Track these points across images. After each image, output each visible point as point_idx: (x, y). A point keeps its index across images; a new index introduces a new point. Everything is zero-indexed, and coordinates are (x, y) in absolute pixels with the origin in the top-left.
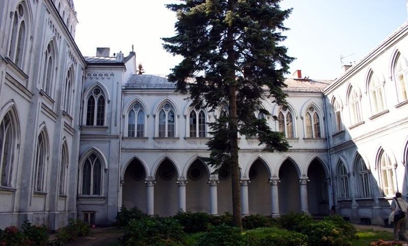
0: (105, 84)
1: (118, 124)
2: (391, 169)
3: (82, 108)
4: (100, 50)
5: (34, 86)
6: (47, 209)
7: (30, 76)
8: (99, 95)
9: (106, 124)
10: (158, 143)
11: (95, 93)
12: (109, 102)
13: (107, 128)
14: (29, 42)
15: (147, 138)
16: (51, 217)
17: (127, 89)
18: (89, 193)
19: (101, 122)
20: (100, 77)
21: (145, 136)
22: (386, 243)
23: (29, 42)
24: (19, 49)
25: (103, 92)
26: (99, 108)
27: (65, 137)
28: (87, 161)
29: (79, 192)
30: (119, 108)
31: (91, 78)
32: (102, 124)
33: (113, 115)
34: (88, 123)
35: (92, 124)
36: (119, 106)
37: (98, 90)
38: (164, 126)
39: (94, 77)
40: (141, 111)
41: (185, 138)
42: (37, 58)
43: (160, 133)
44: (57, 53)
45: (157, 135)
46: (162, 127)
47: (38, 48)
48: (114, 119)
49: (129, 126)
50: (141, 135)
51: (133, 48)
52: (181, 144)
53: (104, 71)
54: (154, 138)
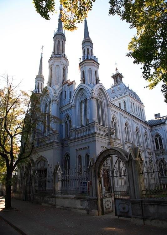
0: (160, 132)
2: (108, 170)
3: (153, 143)
4: (157, 116)
6: (148, 183)
8: (159, 137)
12: (163, 139)
14: (130, 133)
16: (149, 186)
18: (163, 176)
20: (157, 130)
22: (10, 163)
23: (130, 133)
24: (128, 136)
26: (160, 142)
28: (160, 163)
29: (159, 176)
31: (154, 131)
34: (157, 149)
37: (158, 135)
42: (133, 136)
48: (95, 189)
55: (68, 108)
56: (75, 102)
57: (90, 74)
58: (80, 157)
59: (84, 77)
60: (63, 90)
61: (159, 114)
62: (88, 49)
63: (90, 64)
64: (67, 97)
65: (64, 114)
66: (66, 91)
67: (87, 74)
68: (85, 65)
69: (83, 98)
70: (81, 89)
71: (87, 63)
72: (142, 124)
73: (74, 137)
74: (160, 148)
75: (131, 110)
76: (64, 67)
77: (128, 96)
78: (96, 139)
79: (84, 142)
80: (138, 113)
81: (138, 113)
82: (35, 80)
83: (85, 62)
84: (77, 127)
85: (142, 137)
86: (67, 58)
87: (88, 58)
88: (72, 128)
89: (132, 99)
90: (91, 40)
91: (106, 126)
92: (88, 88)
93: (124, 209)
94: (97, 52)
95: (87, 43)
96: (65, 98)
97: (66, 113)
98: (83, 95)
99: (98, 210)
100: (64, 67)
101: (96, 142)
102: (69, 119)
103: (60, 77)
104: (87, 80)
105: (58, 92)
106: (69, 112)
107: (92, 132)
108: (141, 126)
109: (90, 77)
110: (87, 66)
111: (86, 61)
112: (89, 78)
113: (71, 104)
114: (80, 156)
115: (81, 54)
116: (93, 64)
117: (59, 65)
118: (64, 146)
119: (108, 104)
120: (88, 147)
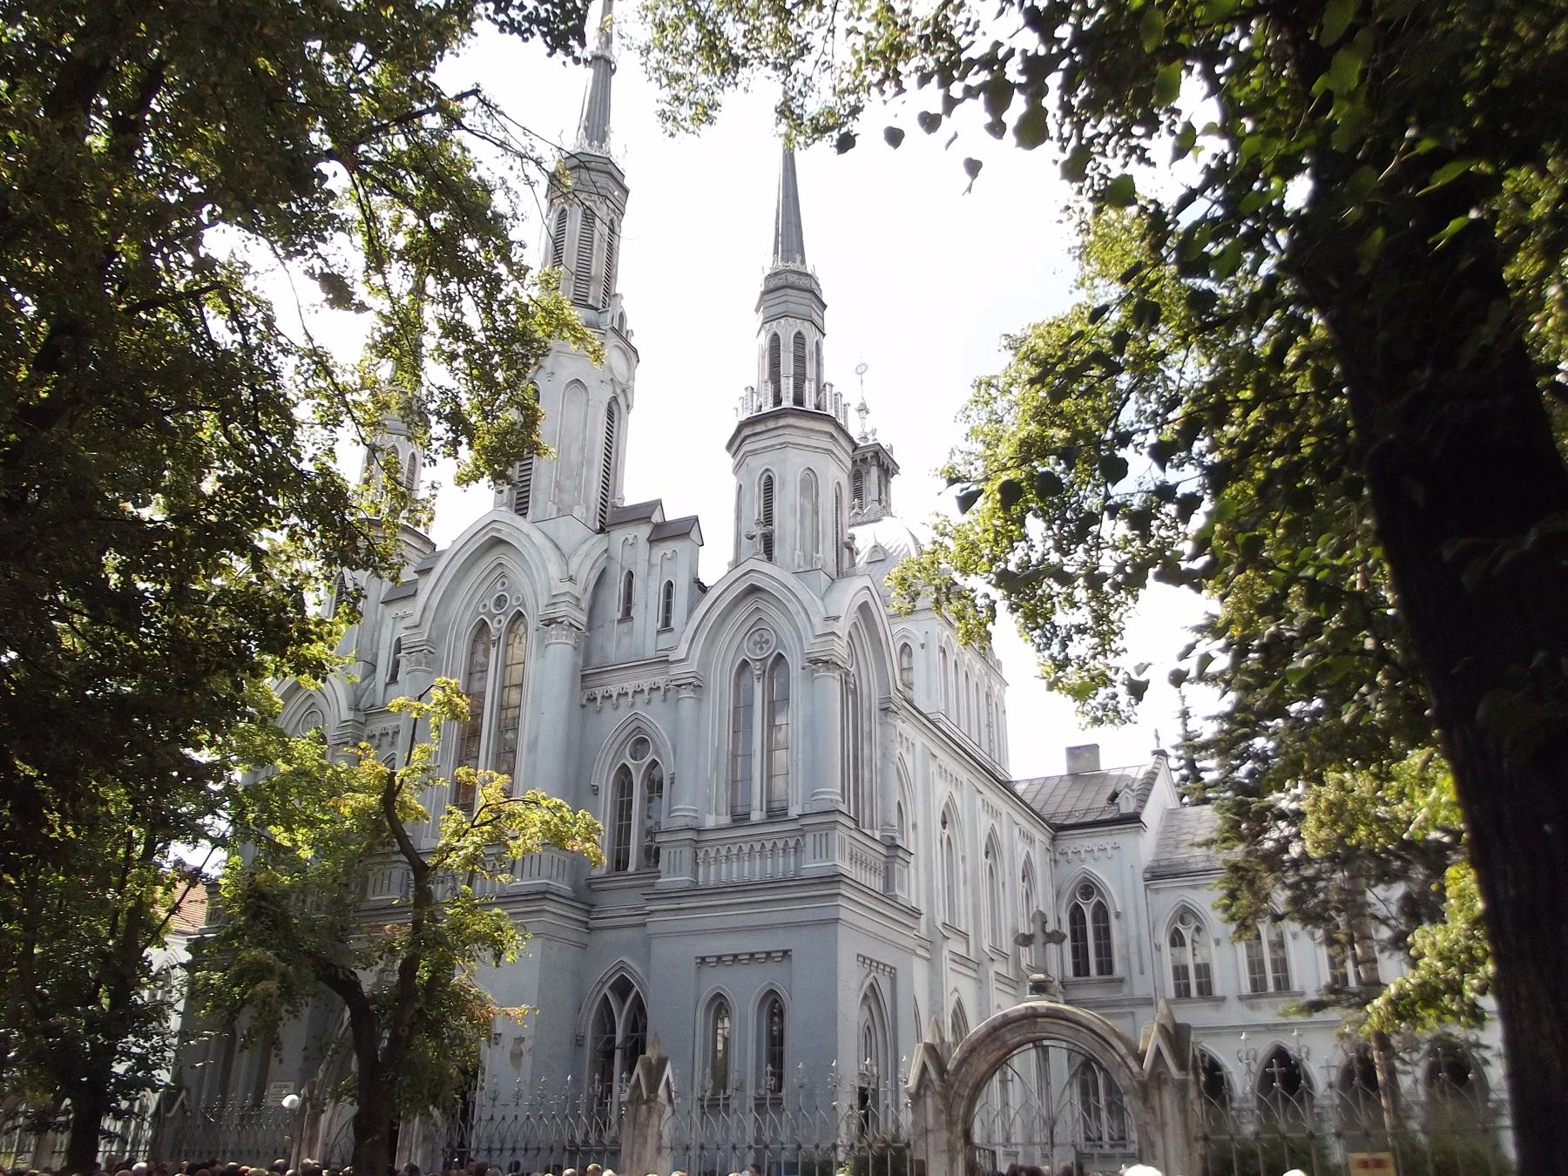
0: (1101, 872)
1: (1148, 970)
5: (979, 949)
7: (971, 933)
9: (1118, 969)
10: (1252, 1007)
11: (1082, 895)
12: (1118, 915)
13: (1121, 980)
15: (1223, 999)
17: (1157, 874)
19: (1106, 967)
21: (1218, 990)
25: (1100, 893)
27: (521, 508)
30: (1145, 932)
32: (1110, 971)
33: (1133, 948)
34: (1077, 973)
35: (1087, 973)
36: (1144, 922)
37: (1088, 888)
38: (1261, 963)
39: (1075, 858)
40: (1198, 930)
41: (1241, 998)
43: (1254, 983)
44: (1001, 853)
45: (1246, 988)
46: (1256, 966)
47: (975, 873)
49: (1176, 969)
50: (1206, 989)
51: (1158, 738)
52: (1235, 1014)
53: (1095, 840)
54: (1241, 998)
55: (630, 687)
56: (705, 664)
57: (809, 506)
60: (609, 558)
62: (799, 338)
63: (814, 441)
65: (612, 722)
66: (630, 574)
67: (787, 500)
68: (785, 445)
70: (754, 590)
73: (683, 879)
75: (942, 707)
76: (615, 399)
78: (843, 914)
80: (963, 712)
81: (963, 712)
83: (782, 422)
84: (710, 821)
85: (1014, 900)
86: (634, 341)
87: (799, 400)
88: (680, 823)
91: (872, 828)
92: (803, 596)
96: (627, 615)
97: (624, 714)
98: (757, 628)
100: (615, 399)
101: (841, 930)
102: (648, 759)
103: (590, 463)
104: (789, 541)
105: (586, 575)
106: (656, 718)
107: (812, 865)
108: (982, 815)
109: (808, 522)
111: (791, 421)
112: (802, 523)
113: (675, 670)
115: (748, 368)
116: (826, 443)
118: (593, 923)
119: (889, 700)
120: (785, 953)
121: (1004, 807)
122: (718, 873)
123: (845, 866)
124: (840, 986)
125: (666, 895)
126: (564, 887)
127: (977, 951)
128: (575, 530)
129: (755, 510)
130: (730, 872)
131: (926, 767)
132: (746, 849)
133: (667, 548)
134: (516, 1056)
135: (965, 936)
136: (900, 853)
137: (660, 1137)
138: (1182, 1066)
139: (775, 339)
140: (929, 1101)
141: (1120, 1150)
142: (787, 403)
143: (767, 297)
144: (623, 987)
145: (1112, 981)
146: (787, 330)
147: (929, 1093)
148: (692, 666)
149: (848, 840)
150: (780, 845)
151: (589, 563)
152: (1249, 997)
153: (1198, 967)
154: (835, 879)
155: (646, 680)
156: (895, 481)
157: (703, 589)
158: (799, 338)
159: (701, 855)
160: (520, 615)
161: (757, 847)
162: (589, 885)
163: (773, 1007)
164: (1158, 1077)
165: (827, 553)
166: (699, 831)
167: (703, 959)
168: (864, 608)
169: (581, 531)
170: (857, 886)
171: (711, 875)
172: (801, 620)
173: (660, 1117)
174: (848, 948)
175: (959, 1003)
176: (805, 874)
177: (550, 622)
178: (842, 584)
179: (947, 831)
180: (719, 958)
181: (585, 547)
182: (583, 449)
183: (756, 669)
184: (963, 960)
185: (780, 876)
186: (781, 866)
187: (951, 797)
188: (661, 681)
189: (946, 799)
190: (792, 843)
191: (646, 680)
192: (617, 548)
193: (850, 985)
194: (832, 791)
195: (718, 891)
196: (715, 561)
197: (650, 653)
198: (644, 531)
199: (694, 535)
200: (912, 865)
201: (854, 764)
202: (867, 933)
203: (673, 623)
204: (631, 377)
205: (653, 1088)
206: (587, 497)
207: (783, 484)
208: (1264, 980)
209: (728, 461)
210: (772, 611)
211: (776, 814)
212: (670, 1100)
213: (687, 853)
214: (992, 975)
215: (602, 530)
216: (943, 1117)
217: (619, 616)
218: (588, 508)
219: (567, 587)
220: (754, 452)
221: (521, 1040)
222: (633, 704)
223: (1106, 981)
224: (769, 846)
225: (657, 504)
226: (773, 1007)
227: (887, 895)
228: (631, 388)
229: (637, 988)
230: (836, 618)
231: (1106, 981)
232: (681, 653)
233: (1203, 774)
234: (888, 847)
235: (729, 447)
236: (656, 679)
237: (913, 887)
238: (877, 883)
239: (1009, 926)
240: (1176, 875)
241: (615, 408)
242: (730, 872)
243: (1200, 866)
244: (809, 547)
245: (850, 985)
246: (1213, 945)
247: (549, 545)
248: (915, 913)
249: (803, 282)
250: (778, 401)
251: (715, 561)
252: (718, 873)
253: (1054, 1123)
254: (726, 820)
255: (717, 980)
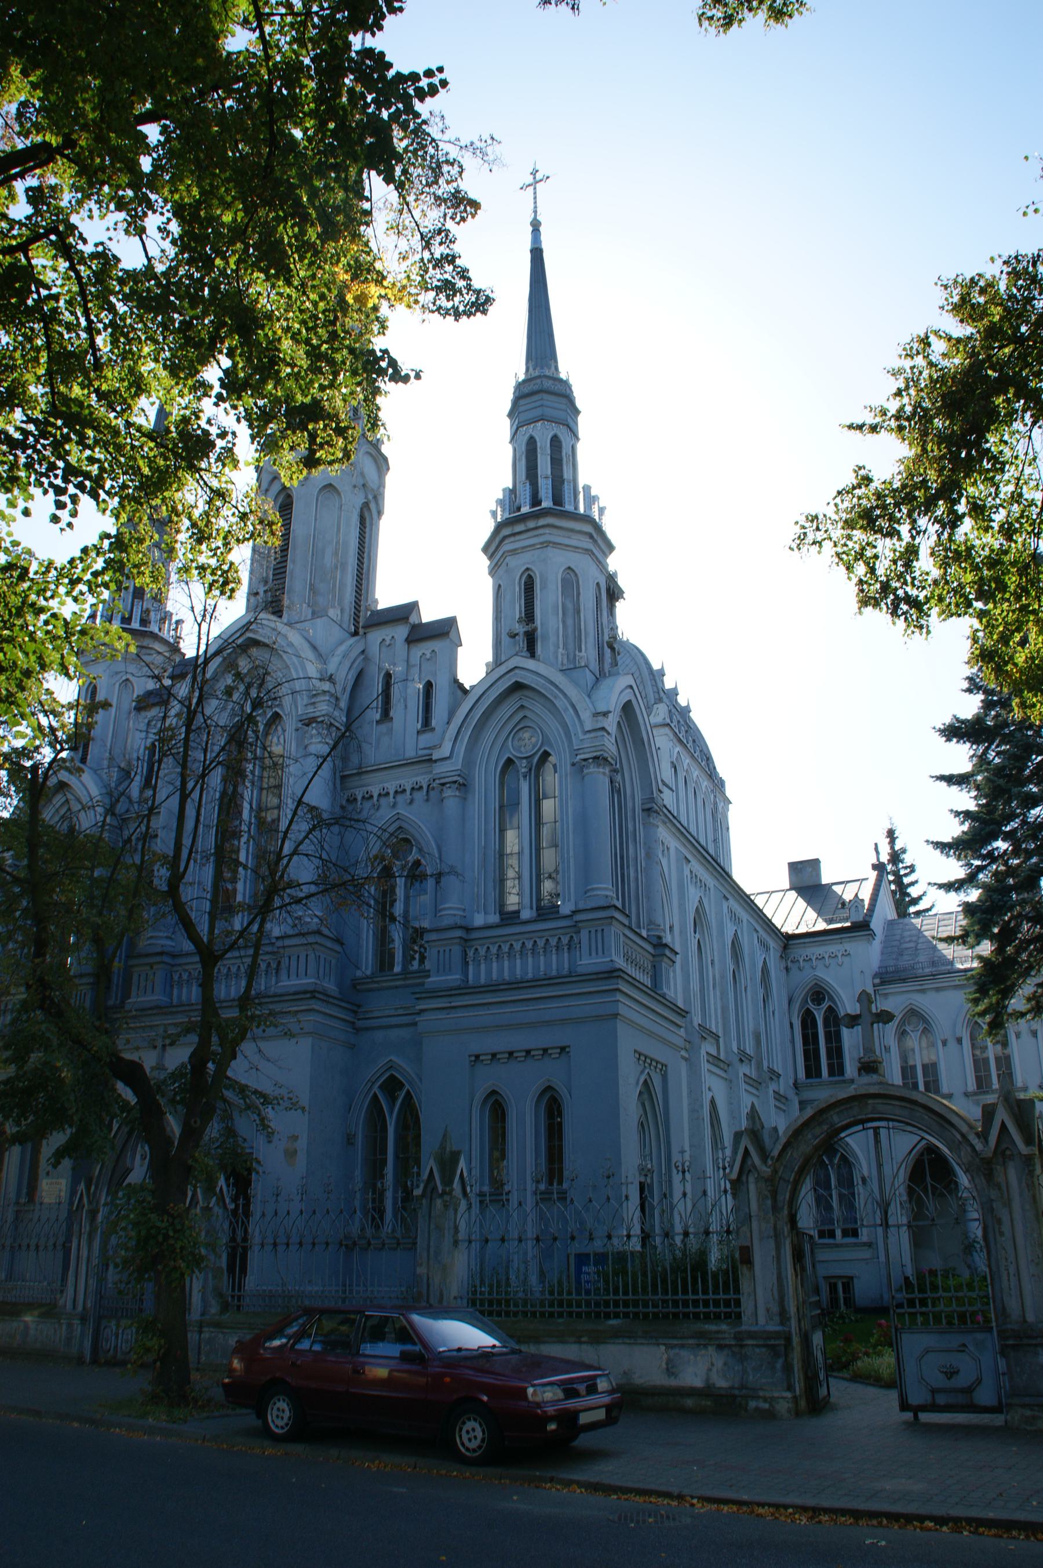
8: (825, 1005)
11: (813, 1001)
25: (831, 999)
32: (841, 1072)
34: (808, 1075)
35: (819, 1075)
37: (819, 994)
41: (966, 1095)
43: (979, 1080)
45: (972, 1086)
54: (966, 1095)
56: (469, 761)
57: (570, 606)
58: (497, 1109)
59: (529, 616)
60: (366, 659)
61: (815, 864)
62: (556, 443)
64: (396, 712)
68: (546, 544)
69: (528, 743)
70: (518, 687)
71: (554, 531)
72: (759, 929)
73: (454, 978)
74: (921, 1088)
77: (667, 730)
78: (622, 1010)
79: (655, 1028)
82: (505, 427)
83: (542, 522)
84: (479, 920)
86: (385, 449)
89: (693, 764)
90: (566, 384)
93: (951, 1373)
94: (602, 466)
95: (543, 406)
99: (790, 1388)
104: (552, 639)
105: (345, 677)
107: (587, 962)
109: (570, 622)
110: (551, 552)
111: (550, 520)
112: (564, 622)
113: (440, 769)
114: (493, 1098)
117: (344, 488)
118: (359, 1024)
120: (563, 1049)
121: (744, 916)
122: (489, 972)
123: (620, 963)
124: (621, 1082)
125: (434, 994)
126: (330, 986)
127: (726, 1052)
128: (329, 630)
129: (517, 610)
130: (501, 970)
131: (680, 871)
132: (517, 946)
133: (425, 648)
134: (291, 1154)
135: (716, 1037)
136: (667, 952)
137: (456, 1229)
138: (1029, 1141)
139: (532, 442)
140: (752, 1187)
141: (851, 1240)
142: (547, 503)
143: (522, 402)
144: (392, 1085)
145: (844, 1082)
146: (543, 434)
147: (751, 1179)
148: (457, 764)
149: (622, 938)
150: (553, 942)
151: (347, 664)
152: (975, 1094)
153: (925, 1067)
154: (613, 974)
155: (407, 779)
156: (620, 605)
157: (465, 692)
158: (556, 443)
159: (471, 953)
160: (276, 716)
161: (529, 945)
162: (354, 986)
163: (552, 1106)
164: (1003, 1151)
165: (589, 653)
166: (468, 930)
167: (477, 1057)
168: (627, 708)
169: (337, 633)
170: (633, 983)
171: (481, 973)
172: (569, 716)
173: (456, 1211)
174: (627, 1042)
175: (713, 1102)
176: (580, 970)
177: (309, 722)
178: (606, 683)
179: (697, 936)
180: (494, 1055)
181: (343, 648)
182: (336, 553)
183: (522, 767)
184: (715, 1060)
185: (554, 973)
186: (554, 963)
187: (700, 902)
188: (423, 780)
189: (696, 904)
190: (565, 940)
191: (407, 779)
192: (374, 650)
193: (629, 1078)
194: (605, 889)
195: (493, 988)
196: (473, 662)
197: (410, 753)
198: (401, 632)
199: (452, 634)
200: (678, 965)
201: (621, 862)
202: (642, 1029)
203: (434, 723)
204: (382, 485)
205: (448, 1181)
206: (341, 600)
207: (544, 587)
208: (989, 1076)
209: (485, 562)
210: (537, 707)
211: (546, 912)
212: (465, 1194)
213: (457, 950)
214: (741, 1075)
215: (356, 633)
216: (769, 1202)
217: (378, 717)
218: (342, 611)
219: (326, 686)
220: (514, 552)
221: (295, 1138)
222: (394, 805)
223: (837, 1082)
224: (541, 943)
225: (412, 607)
226: (552, 1106)
227: (655, 990)
228: (382, 495)
229: (407, 1086)
230: (605, 714)
231: (837, 1082)
232: (445, 750)
233: (909, 890)
234: (655, 946)
235: (485, 550)
236: (419, 779)
237: (676, 986)
238: (648, 982)
239: (751, 1029)
240: (904, 980)
241: (366, 514)
242: (501, 970)
243: (927, 971)
244: (571, 646)
245: (629, 1078)
246: (940, 1044)
247: (306, 645)
248: (683, 1013)
249: (558, 388)
250: (536, 501)
251: (473, 662)
252: (489, 972)
253: (888, 1205)
254: (494, 918)
255: (488, 1078)
